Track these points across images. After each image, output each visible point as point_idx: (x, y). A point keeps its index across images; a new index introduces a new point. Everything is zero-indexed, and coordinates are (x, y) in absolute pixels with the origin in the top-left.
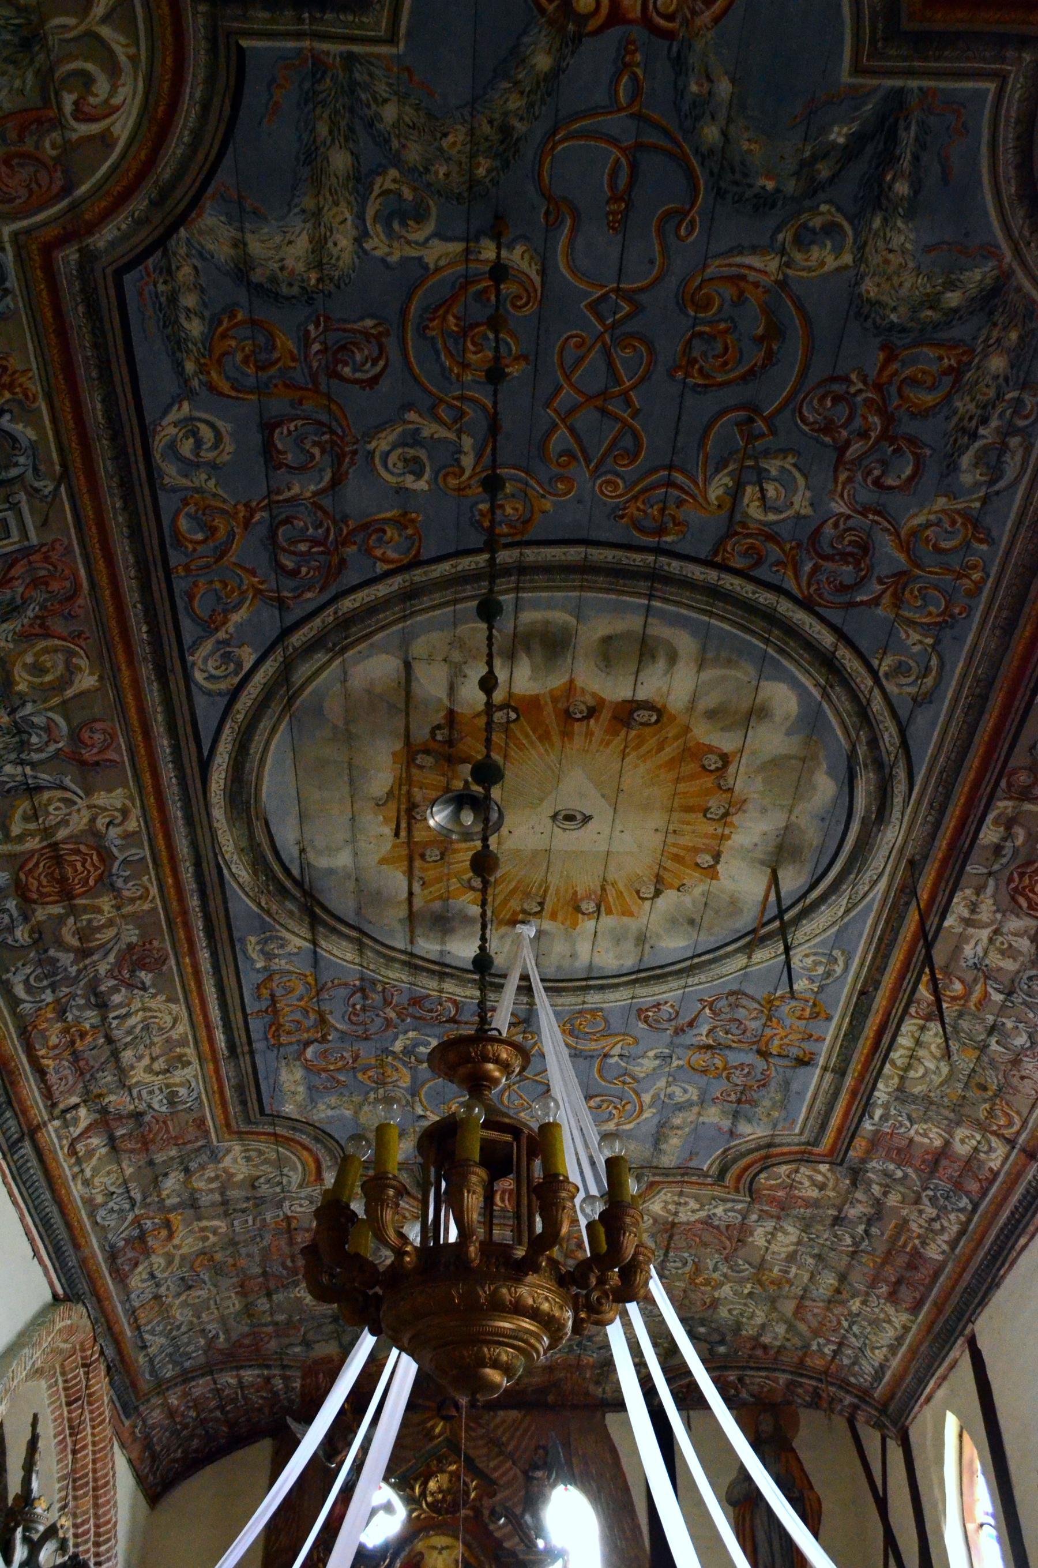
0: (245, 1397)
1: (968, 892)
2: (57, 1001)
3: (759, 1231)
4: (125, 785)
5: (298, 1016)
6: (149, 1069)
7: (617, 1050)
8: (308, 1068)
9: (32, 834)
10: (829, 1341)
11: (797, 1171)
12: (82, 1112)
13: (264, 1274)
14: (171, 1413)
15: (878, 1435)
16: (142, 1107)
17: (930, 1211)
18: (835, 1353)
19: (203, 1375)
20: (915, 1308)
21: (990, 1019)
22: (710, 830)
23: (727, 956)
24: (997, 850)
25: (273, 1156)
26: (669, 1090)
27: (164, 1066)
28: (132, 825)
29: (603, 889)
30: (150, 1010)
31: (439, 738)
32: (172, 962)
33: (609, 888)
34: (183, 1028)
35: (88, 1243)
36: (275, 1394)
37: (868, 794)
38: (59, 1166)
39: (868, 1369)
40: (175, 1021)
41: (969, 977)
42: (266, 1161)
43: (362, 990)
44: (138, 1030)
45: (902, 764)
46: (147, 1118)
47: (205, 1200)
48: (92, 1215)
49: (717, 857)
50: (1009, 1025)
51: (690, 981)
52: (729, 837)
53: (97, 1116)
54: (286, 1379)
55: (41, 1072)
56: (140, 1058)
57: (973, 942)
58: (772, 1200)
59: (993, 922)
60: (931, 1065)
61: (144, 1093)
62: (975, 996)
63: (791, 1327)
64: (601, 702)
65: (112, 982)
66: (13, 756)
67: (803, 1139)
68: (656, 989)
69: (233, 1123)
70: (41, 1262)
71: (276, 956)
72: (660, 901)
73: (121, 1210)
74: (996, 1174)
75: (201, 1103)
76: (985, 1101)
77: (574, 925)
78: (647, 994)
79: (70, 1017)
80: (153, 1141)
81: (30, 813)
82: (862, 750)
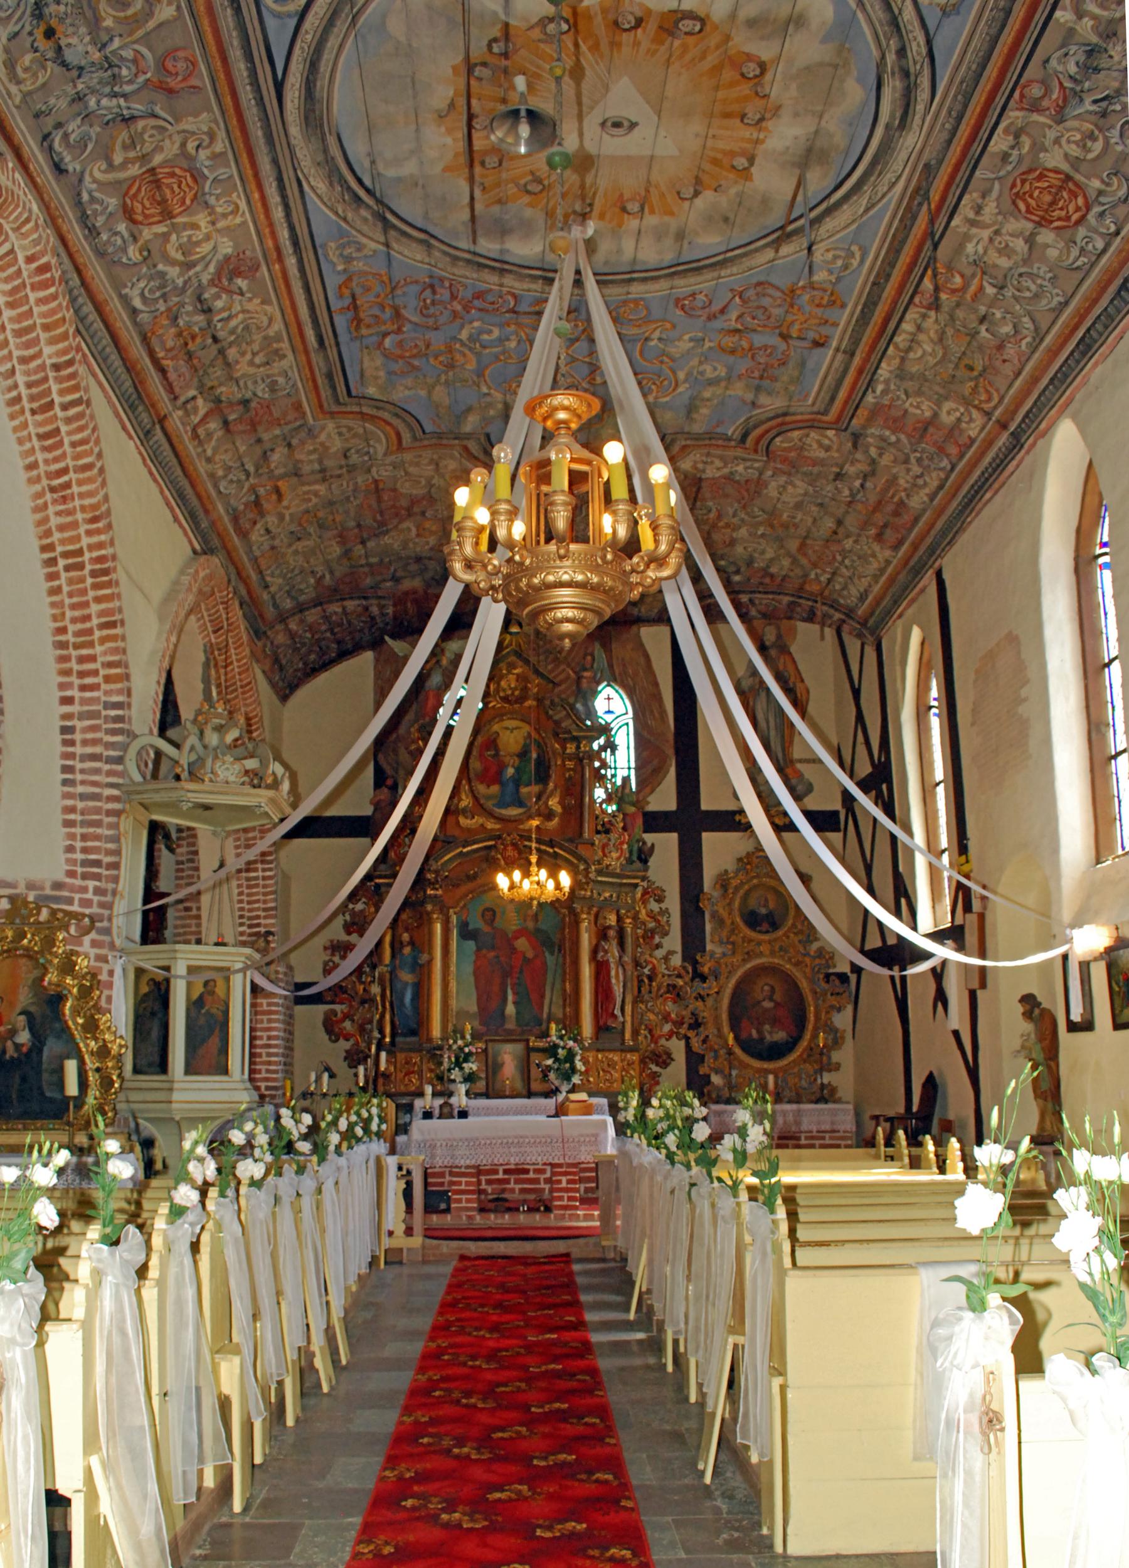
0: (349, 623)
1: (975, 195)
2: (169, 310)
3: (773, 484)
4: (209, 110)
5: (376, 311)
6: (251, 363)
7: (657, 334)
8: (387, 355)
9: (132, 161)
10: (824, 571)
11: (807, 435)
12: (200, 402)
13: (359, 526)
14: (292, 635)
15: (859, 643)
16: (249, 395)
17: (916, 470)
18: (829, 581)
19: (315, 606)
20: (896, 547)
21: (983, 309)
22: (747, 134)
23: (757, 250)
24: (1005, 157)
25: (361, 431)
26: (701, 368)
27: (264, 360)
28: (219, 147)
29: (647, 191)
30: (248, 312)
31: (496, 50)
32: (264, 268)
33: (652, 190)
34: (278, 326)
35: (215, 508)
36: (373, 618)
37: (893, 102)
38: (186, 448)
39: (854, 591)
40: (271, 320)
41: (968, 272)
42: (355, 435)
43: (432, 286)
44: (239, 330)
45: (927, 72)
46: (253, 404)
47: (306, 469)
48: (216, 486)
49: (751, 160)
50: (998, 315)
51: (723, 273)
52: (763, 142)
53: (212, 405)
54: (382, 607)
55: (163, 371)
56: (243, 354)
57: (975, 241)
58: (784, 460)
59: (994, 223)
60: (929, 349)
61: (249, 383)
62: (973, 288)
63: (795, 561)
64: (649, 12)
65: (214, 290)
66: (107, 90)
67: (815, 409)
68: (692, 280)
69: (325, 405)
70: (181, 526)
71: (353, 259)
72: (699, 202)
73: (239, 481)
74: (972, 441)
75: (297, 390)
76: (971, 379)
77: (620, 225)
78: (684, 286)
79: (181, 323)
80: (260, 423)
81: (128, 142)
82: (891, 58)
